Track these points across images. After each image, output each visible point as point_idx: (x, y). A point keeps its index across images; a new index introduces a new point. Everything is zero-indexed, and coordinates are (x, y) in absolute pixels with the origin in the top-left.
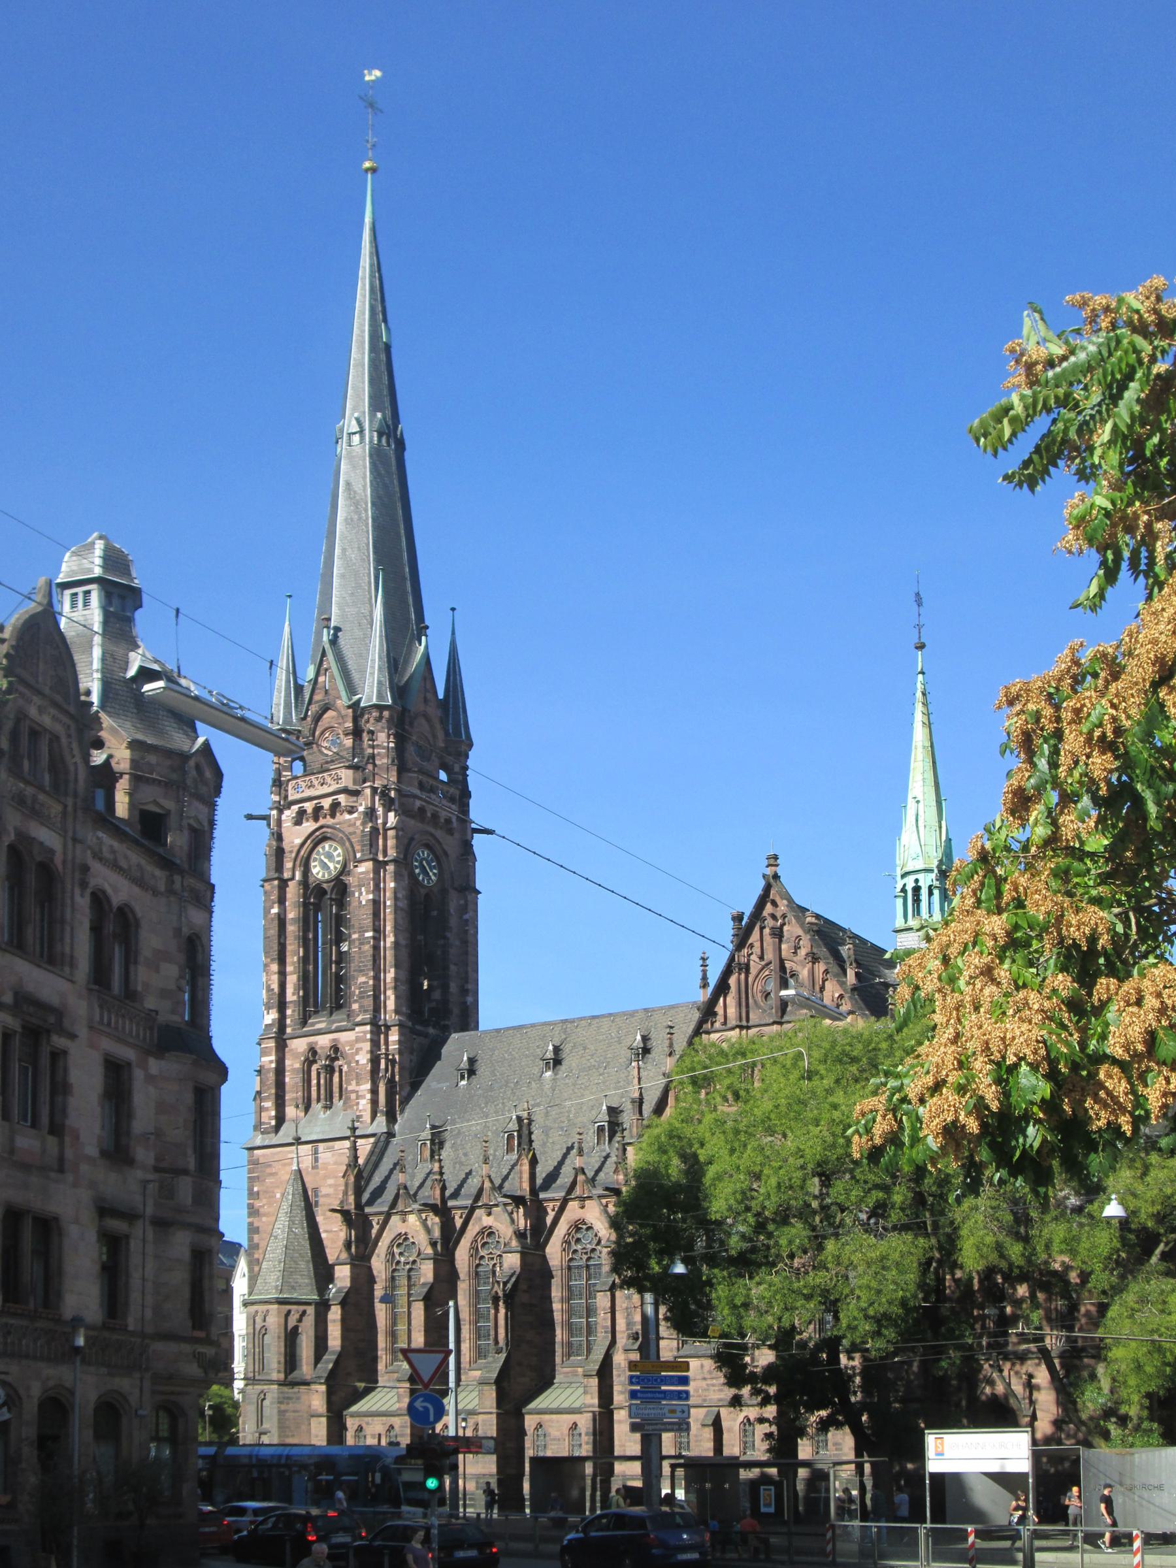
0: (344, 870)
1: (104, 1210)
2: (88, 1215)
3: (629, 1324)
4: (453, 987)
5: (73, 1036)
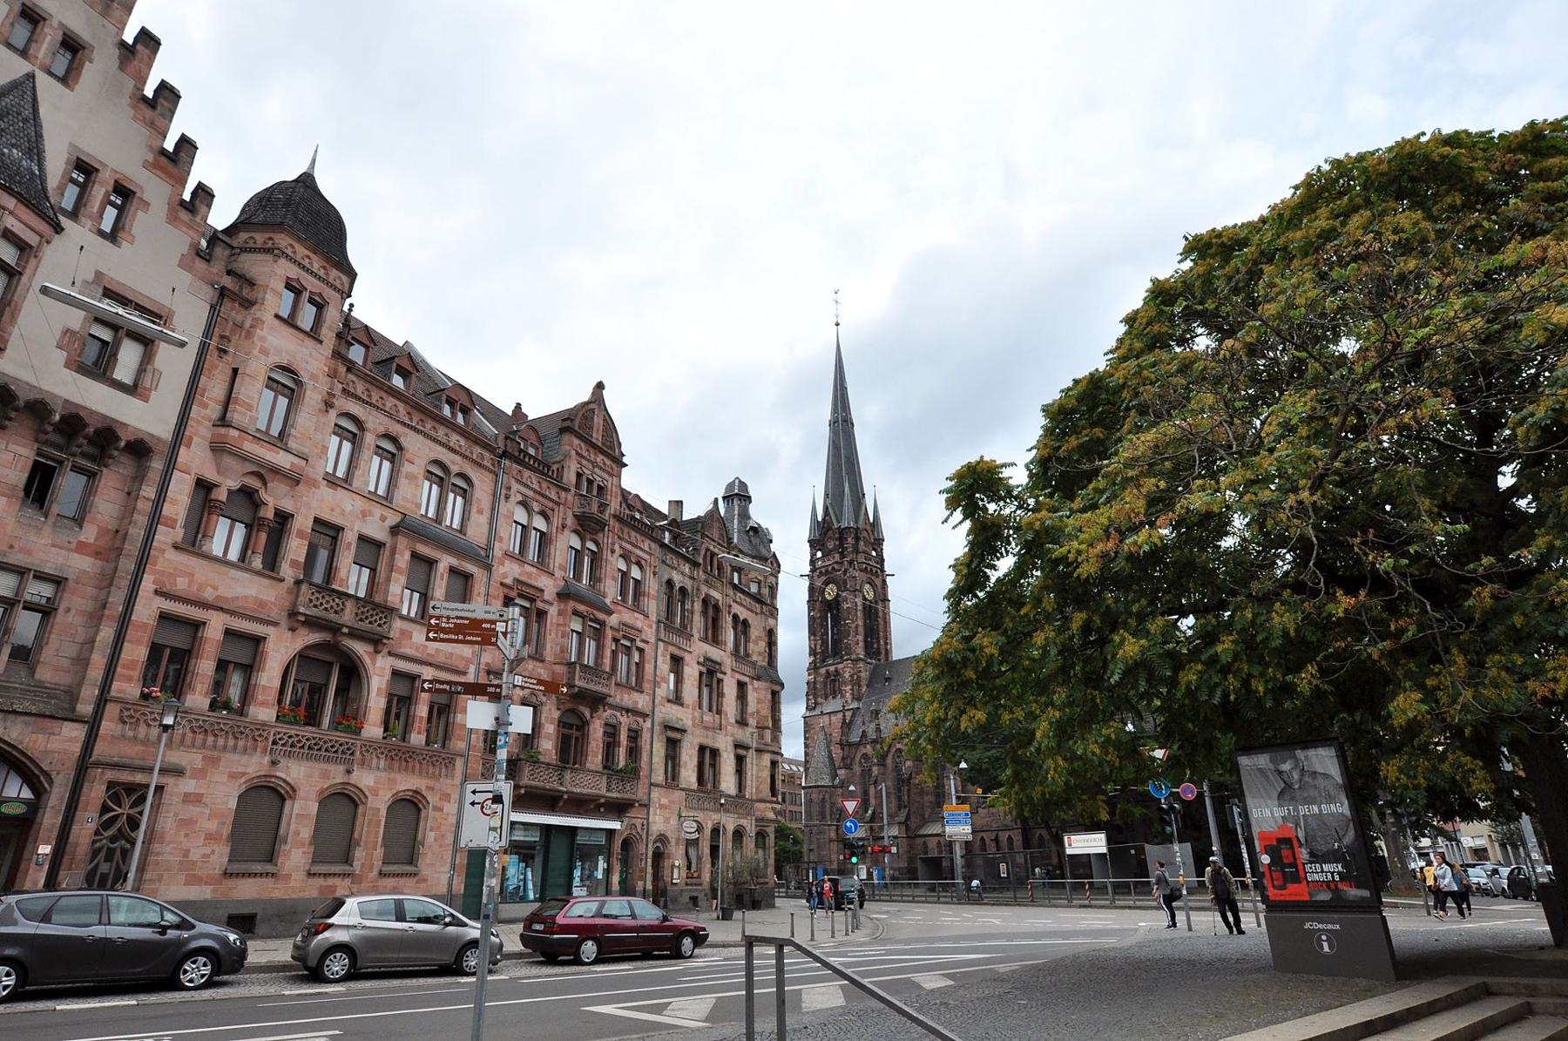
1: (737, 746)
2: (730, 748)
4: (882, 642)
5: (725, 674)
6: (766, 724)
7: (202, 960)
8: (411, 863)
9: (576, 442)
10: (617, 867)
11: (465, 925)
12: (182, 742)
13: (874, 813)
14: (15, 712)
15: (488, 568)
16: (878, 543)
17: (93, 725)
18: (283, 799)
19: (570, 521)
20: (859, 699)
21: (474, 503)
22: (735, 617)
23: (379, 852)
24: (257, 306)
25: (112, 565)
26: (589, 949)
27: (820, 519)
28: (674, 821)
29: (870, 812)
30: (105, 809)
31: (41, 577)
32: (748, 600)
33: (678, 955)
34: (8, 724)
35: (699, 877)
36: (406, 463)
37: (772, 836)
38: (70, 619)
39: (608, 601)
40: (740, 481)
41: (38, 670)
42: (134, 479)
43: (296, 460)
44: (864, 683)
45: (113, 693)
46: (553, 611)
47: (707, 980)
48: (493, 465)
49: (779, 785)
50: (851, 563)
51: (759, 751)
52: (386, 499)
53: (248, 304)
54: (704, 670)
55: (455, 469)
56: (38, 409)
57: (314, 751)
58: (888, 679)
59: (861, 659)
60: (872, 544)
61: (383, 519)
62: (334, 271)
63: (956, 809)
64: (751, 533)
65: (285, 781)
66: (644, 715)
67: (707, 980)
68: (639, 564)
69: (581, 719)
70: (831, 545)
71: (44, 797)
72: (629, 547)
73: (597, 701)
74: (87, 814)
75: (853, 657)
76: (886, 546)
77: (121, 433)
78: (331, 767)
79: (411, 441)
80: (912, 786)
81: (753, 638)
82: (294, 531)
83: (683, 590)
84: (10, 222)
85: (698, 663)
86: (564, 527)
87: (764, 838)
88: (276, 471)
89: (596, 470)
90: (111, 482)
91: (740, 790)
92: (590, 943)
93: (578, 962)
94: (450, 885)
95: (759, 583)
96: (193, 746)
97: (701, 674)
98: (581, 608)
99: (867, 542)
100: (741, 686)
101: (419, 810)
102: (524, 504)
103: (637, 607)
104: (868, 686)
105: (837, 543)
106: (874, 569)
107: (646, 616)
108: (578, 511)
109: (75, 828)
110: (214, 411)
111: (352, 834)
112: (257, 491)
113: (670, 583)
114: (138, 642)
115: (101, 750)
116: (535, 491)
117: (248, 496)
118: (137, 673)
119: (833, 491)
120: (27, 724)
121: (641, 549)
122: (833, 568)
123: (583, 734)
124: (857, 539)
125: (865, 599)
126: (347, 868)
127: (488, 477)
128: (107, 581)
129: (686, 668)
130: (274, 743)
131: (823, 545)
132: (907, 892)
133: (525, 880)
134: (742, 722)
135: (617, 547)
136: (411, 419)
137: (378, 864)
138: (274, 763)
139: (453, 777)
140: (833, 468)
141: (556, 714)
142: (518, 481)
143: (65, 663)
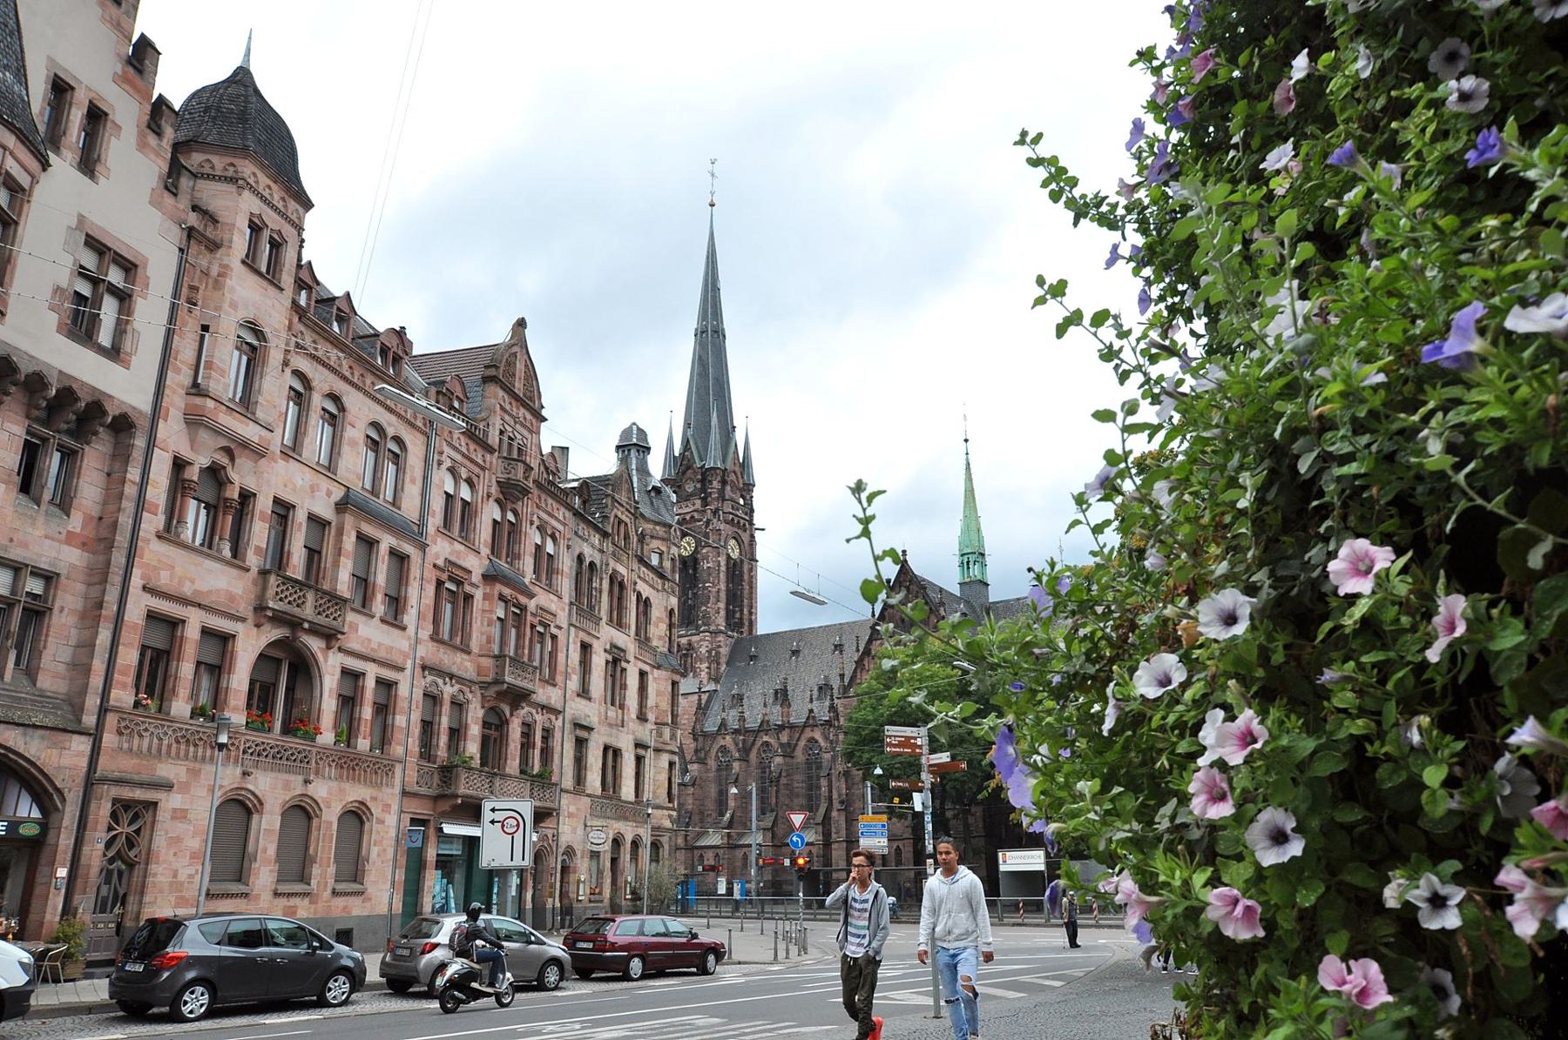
0: (696, 551)
1: (638, 745)
2: (631, 746)
3: (840, 795)
5: (628, 662)
6: (665, 720)
7: (200, 989)
8: (239, 880)
9: (501, 393)
10: (530, 883)
11: (544, 943)
12: (169, 753)
13: (732, 816)
14: (35, 726)
15: (423, 547)
16: (747, 488)
17: (96, 736)
18: (249, 813)
19: (494, 490)
20: (717, 680)
21: (408, 471)
22: (639, 595)
23: (332, 870)
24: (221, 251)
25: (101, 558)
26: (636, 966)
27: (677, 454)
28: (580, 831)
29: (728, 815)
30: (110, 829)
31: (37, 573)
32: (651, 575)
33: (704, 971)
34: (28, 739)
35: (600, 893)
36: (349, 427)
37: (666, 847)
38: (63, 620)
39: (527, 581)
40: (639, 429)
41: (40, 677)
42: (114, 456)
43: (264, 433)
44: (723, 660)
45: (111, 703)
46: (478, 595)
47: (818, 988)
48: (425, 425)
49: (675, 791)
50: (715, 512)
51: (657, 750)
52: (329, 469)
53: (214, 246)
54: (610, 658)
55: (391, 432)
56: (36, 382)
57: (279, 759)
58: (753, 658)
59: (721, 632)
60: (740, 490)
61: (329, 494)
62: (293, 202)
63: (873, 820)
64: (653, 494)
65: (253, 794)
66: (556, 712)
67: (818, 988)
68: (553, 537)
69: (500, 718)
70: (689, 488)
71: (54, 817)
72: (545, 516)
73: (518, 697)
74: (98, 835)
75: (712, 628)
76: (756, 493)
77: (80, 394)
78: (292, 777)
79: (353, 399)
80: (782, 787)
81: (654, 619)
82: (257, 512)
83: (592, 564)
84: (11, 165)
85: (605, 651)
86: (489, 496)
87: (658, 848)
88: (245, 445)
89: (518, 426)
90: (94, 458)
91: (637, 796)
92: (636, 960)
93: (626, 977)
94: (391, 905)
95: (661, 554)
96: (178, 757)
97: (607, 662)
98: (507, 591)
99: (734, 487)
100: (642, 674)
101: (362, 823)
102: (452, 470)
103: (550, 588)
104: (728, 664)
105: (699, 486)
106: (742, 522)
107: (560, 598)
108: (502, 477)
109: (86, 850)
110: (186, 380)
111: (307, 848)
112: (224, 468)
113: (580, 558)
114: (130, 645)
115: (105, 765)
116: (464, 455)
117: (215, 474)
118: (130, 679)
119: (696, 421)
120: (43, 738)
121: (557, 519)
122: (692, 517)
123: (501, 736)
124: (724, 482)
125: (729, 557)
126: (306, 887)
127: (421, 439)
128: (99, 576)
129: (594, 656)
130: (244, 752)
131: (679, 487)
132: (780, 909)
133: (447, 898)
134: (642, 718)
135: (535, 518)
136: (352, 374)
137: (331, 882)
138: (245, 774)
139: (393, 786)
140: (698, 389)
141: (480, 713)
142: (450, 444)
143: (62, 668)
